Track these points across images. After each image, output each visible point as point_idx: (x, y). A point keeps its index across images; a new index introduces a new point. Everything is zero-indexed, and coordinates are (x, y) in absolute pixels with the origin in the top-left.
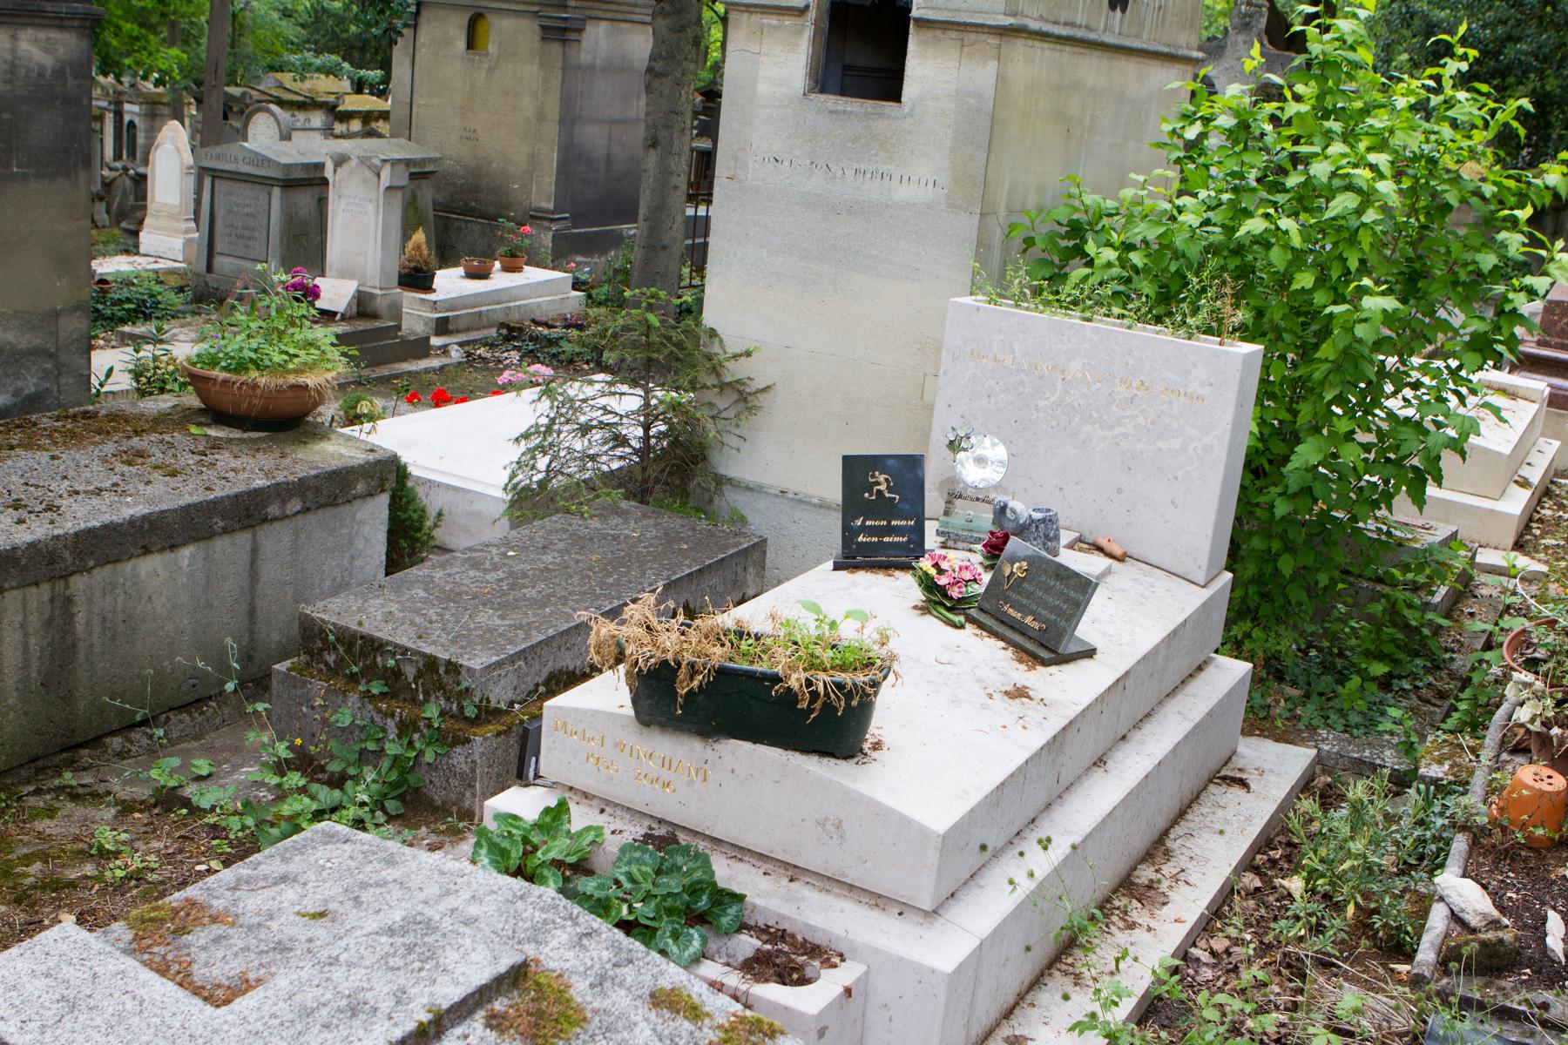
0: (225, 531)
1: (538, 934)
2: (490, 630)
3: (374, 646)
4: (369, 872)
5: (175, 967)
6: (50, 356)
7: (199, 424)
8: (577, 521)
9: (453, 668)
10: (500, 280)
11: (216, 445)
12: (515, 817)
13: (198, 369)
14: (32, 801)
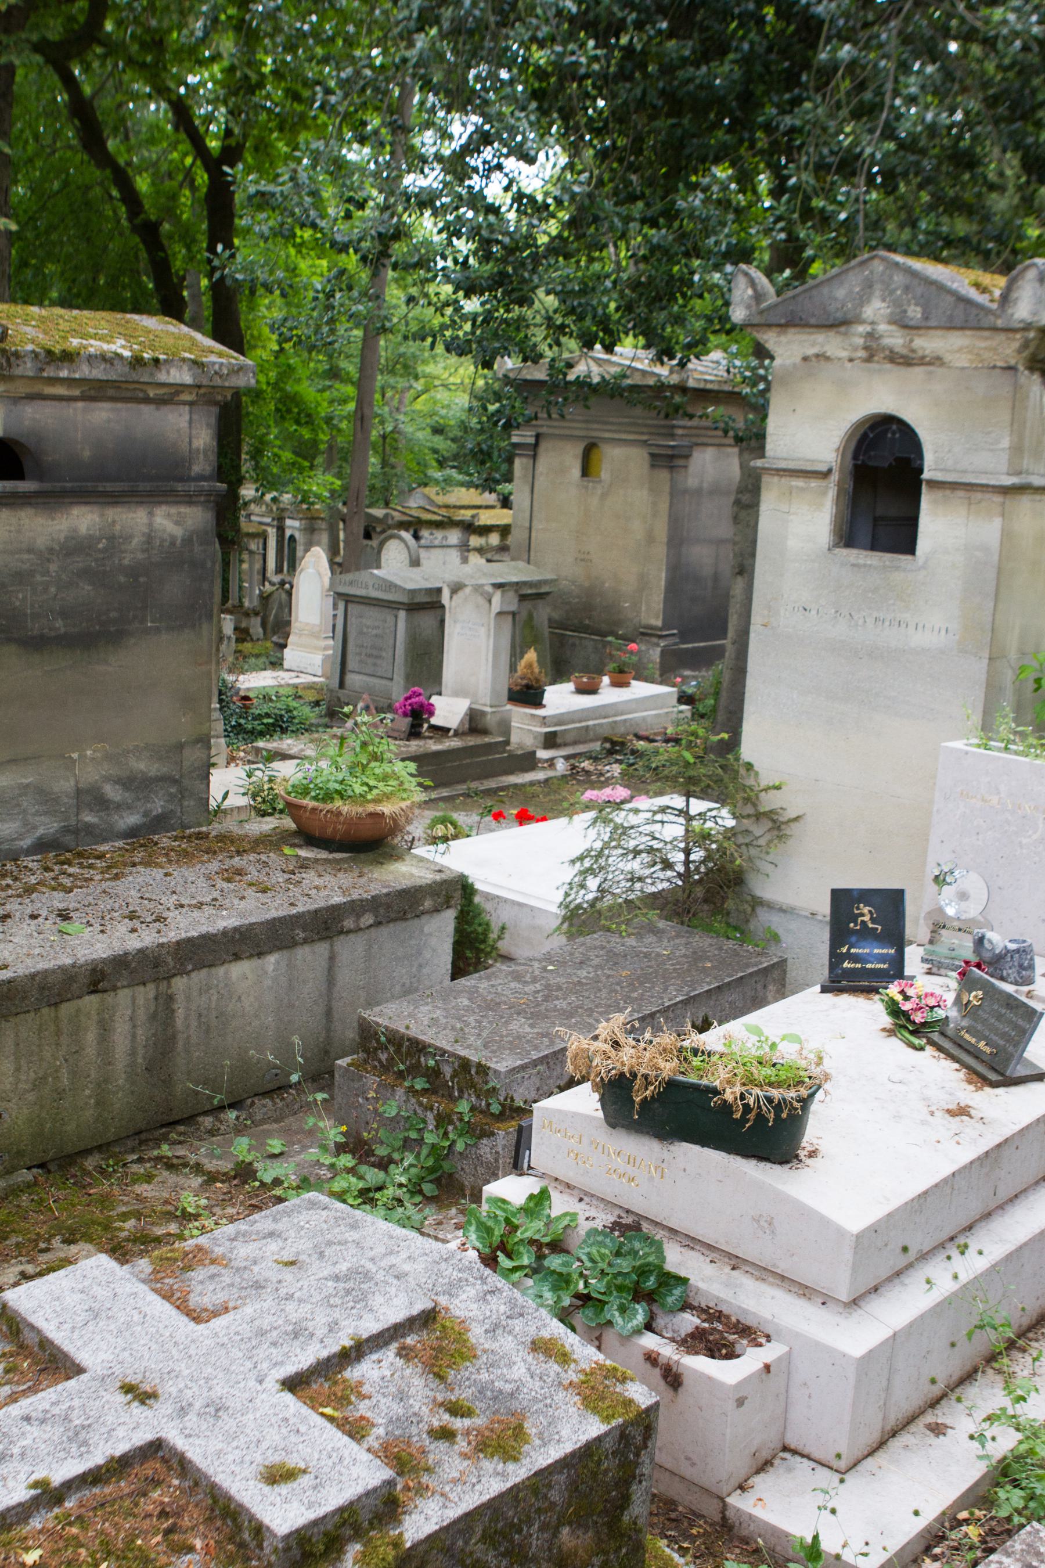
0: (305, 941)
1: (453, 1288)
2: (519, 1037)
3: (418, 1047)
4: (336, 1234)
5: (178, 1295)
6: (175, 782)
7: (293, 846)
8: (615, 939)
9: (483, 1070)
10: (608, 695)
11: (304, 865)
12: (504, 1201)
13: (291, 798)
14: (135, 1168)
